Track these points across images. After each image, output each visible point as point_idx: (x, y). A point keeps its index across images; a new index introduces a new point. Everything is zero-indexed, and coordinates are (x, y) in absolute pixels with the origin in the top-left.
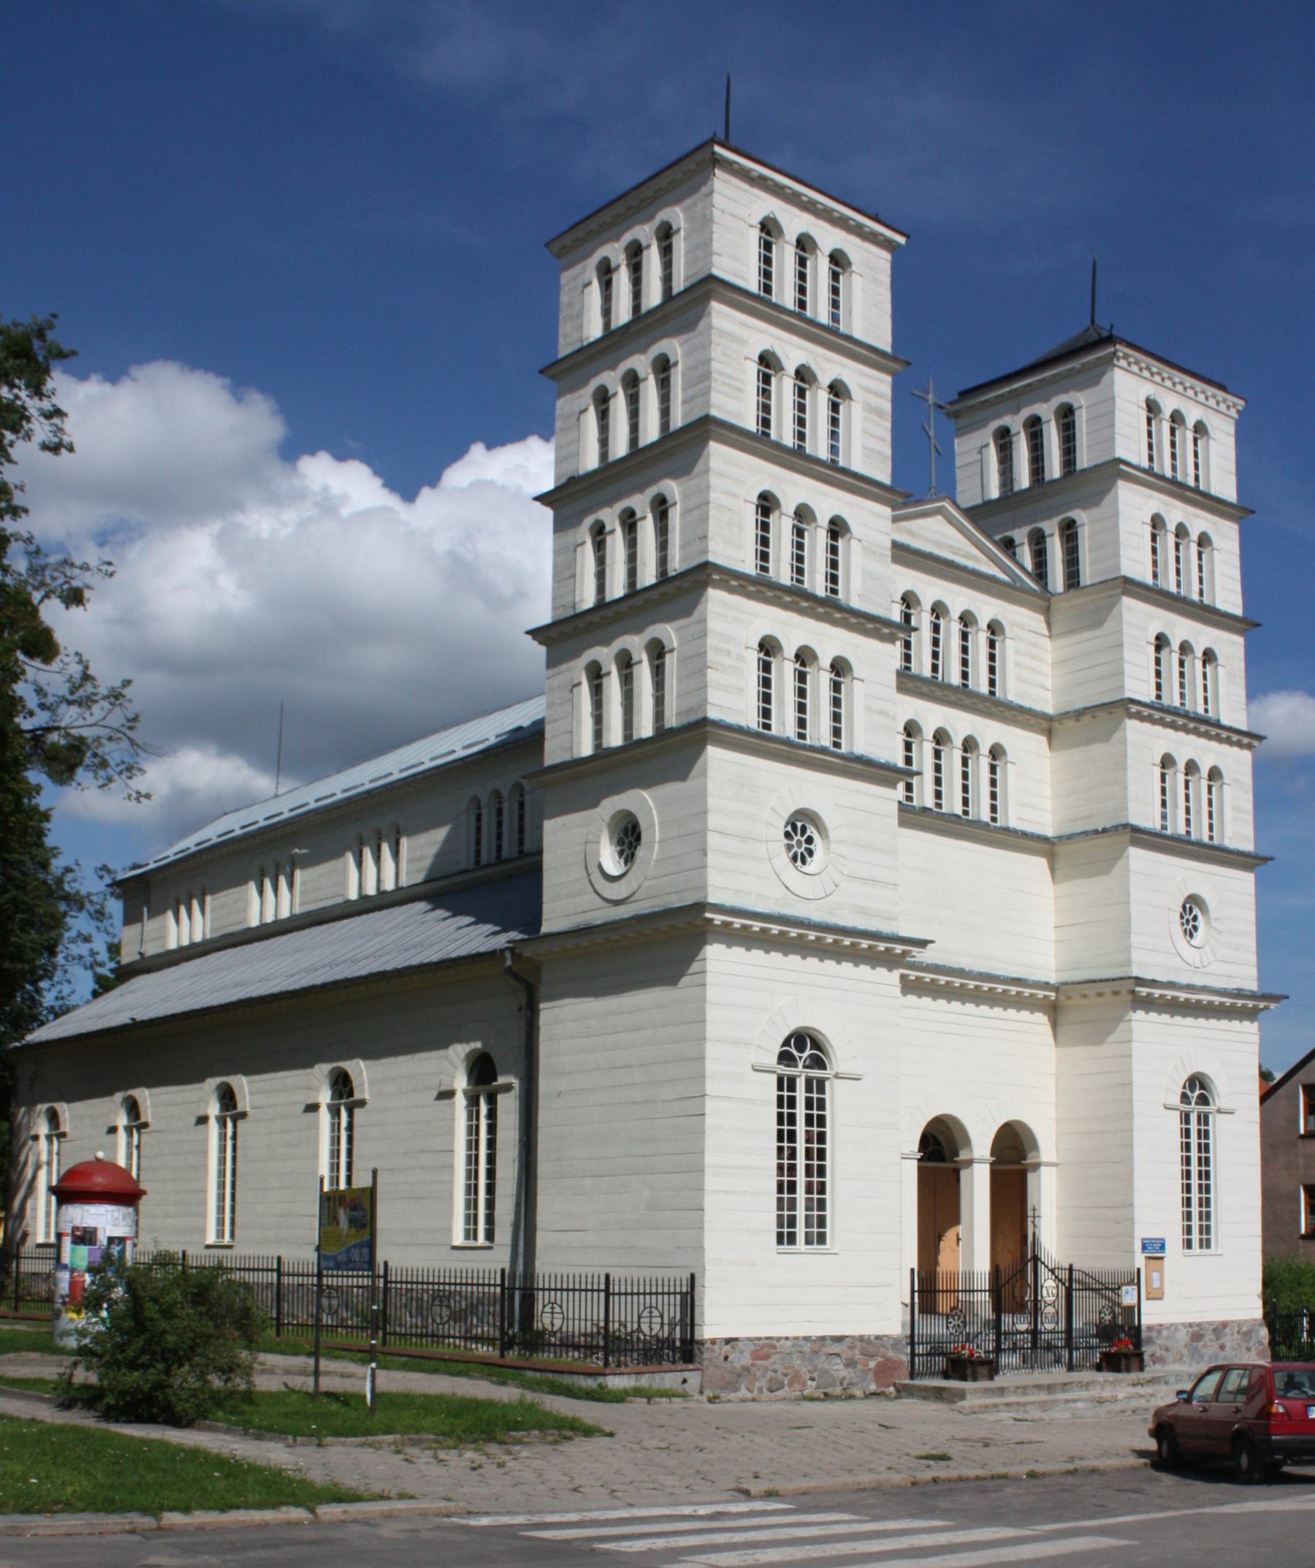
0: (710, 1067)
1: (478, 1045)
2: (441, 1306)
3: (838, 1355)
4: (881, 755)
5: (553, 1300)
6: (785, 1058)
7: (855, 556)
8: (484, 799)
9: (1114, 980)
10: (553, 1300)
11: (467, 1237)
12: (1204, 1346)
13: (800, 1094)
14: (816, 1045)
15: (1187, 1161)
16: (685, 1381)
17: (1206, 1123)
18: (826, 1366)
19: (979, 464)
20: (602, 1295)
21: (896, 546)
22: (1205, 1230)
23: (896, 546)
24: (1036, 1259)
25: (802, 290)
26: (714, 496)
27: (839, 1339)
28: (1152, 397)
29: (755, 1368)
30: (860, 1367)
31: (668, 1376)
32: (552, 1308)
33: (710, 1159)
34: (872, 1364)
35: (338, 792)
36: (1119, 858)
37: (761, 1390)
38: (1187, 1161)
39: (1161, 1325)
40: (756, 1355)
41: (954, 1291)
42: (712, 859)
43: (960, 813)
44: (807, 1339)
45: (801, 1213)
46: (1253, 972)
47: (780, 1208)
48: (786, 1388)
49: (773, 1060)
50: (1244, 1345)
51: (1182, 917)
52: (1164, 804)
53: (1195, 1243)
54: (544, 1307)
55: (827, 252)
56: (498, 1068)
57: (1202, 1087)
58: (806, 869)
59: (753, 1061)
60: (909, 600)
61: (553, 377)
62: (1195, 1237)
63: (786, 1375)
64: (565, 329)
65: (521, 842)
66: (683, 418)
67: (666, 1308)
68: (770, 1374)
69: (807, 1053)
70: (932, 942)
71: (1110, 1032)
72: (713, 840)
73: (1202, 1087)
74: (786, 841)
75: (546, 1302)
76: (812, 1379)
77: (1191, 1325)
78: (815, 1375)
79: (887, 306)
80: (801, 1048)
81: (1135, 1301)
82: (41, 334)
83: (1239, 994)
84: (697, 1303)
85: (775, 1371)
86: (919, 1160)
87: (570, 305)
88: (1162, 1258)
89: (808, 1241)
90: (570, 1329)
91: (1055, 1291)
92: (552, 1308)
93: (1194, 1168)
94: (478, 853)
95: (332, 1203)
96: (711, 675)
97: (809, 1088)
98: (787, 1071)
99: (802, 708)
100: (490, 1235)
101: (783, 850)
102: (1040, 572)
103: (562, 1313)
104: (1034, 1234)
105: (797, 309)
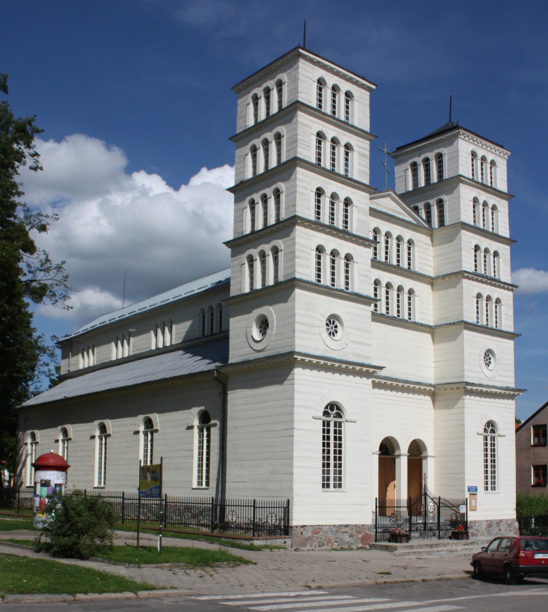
0: (296, 417)
1: (203, 408)
3: (346, 532)
5: (232, 510)
6: (326, 413)
7: (355, 214)
8: (206, 309)
9: (457, 383)
11: (198, 484)
12: (493, 529)
13: (332, 428)
14: (338, 408)
15: (486, 455)
16: (285, 542)
17: (494, 440)
18: (342, 537)
19: (404, 177)
20: (252, 508)
21: (371, 209)
22: (493, 483)
23: (371, 209)
24: (426, 494)
26: (298, 189)
27: (347, 526)
29: (313, 538)
30: (355, 537)
32: (232, 513)
33: (295, 454)
34: (360, 536)
35: (148, 306)
36: (459, 334)
37: (315, 546)
38: (486, 455)
39: (475, 521)
40: (314, 532)
41: (393, 507)
42: (297, 334)
44: (334, 526)
45: (332, 475)
46: (513, 380)
47: (323, 473)
48: (326, 545)
49: (321, 414)
50: (509, 529)
51: (485, 358)
52: (478, 313)
53: (489, 488)
55: (344, 92)
56: (211, 417)
57: (492, 426)
59: (313, 415)
60: (376, 231)
62: (489, 486)
63: (325, 540)
64: (239, 122)
65: (221, 327)
67: (278, 513)
68: (319, 540)
69: (335, 411)
70: (385, 367)
71: (456, 404)
72: (297, 327)
73: (492, 426)
75: (230, 510)
76: (336, 542)
77: (487, 521)
78: (337, 540)
80: (332, 410)
81: (465, 511)
82: (30, 123)
84: (290, 511)
85: (321, 539)
86: (379, 455)
87: (241, 112)
88: (476, 494)
89: (335, 487)
91: (433, 507)
92: (232, 513)
94: (203, 331)
96: (297, 260)
97: (335, 426)
101: (325, 330)
102: (429, 220)
103: (236, 515)
104: (425, 484)
105: (332, 115)
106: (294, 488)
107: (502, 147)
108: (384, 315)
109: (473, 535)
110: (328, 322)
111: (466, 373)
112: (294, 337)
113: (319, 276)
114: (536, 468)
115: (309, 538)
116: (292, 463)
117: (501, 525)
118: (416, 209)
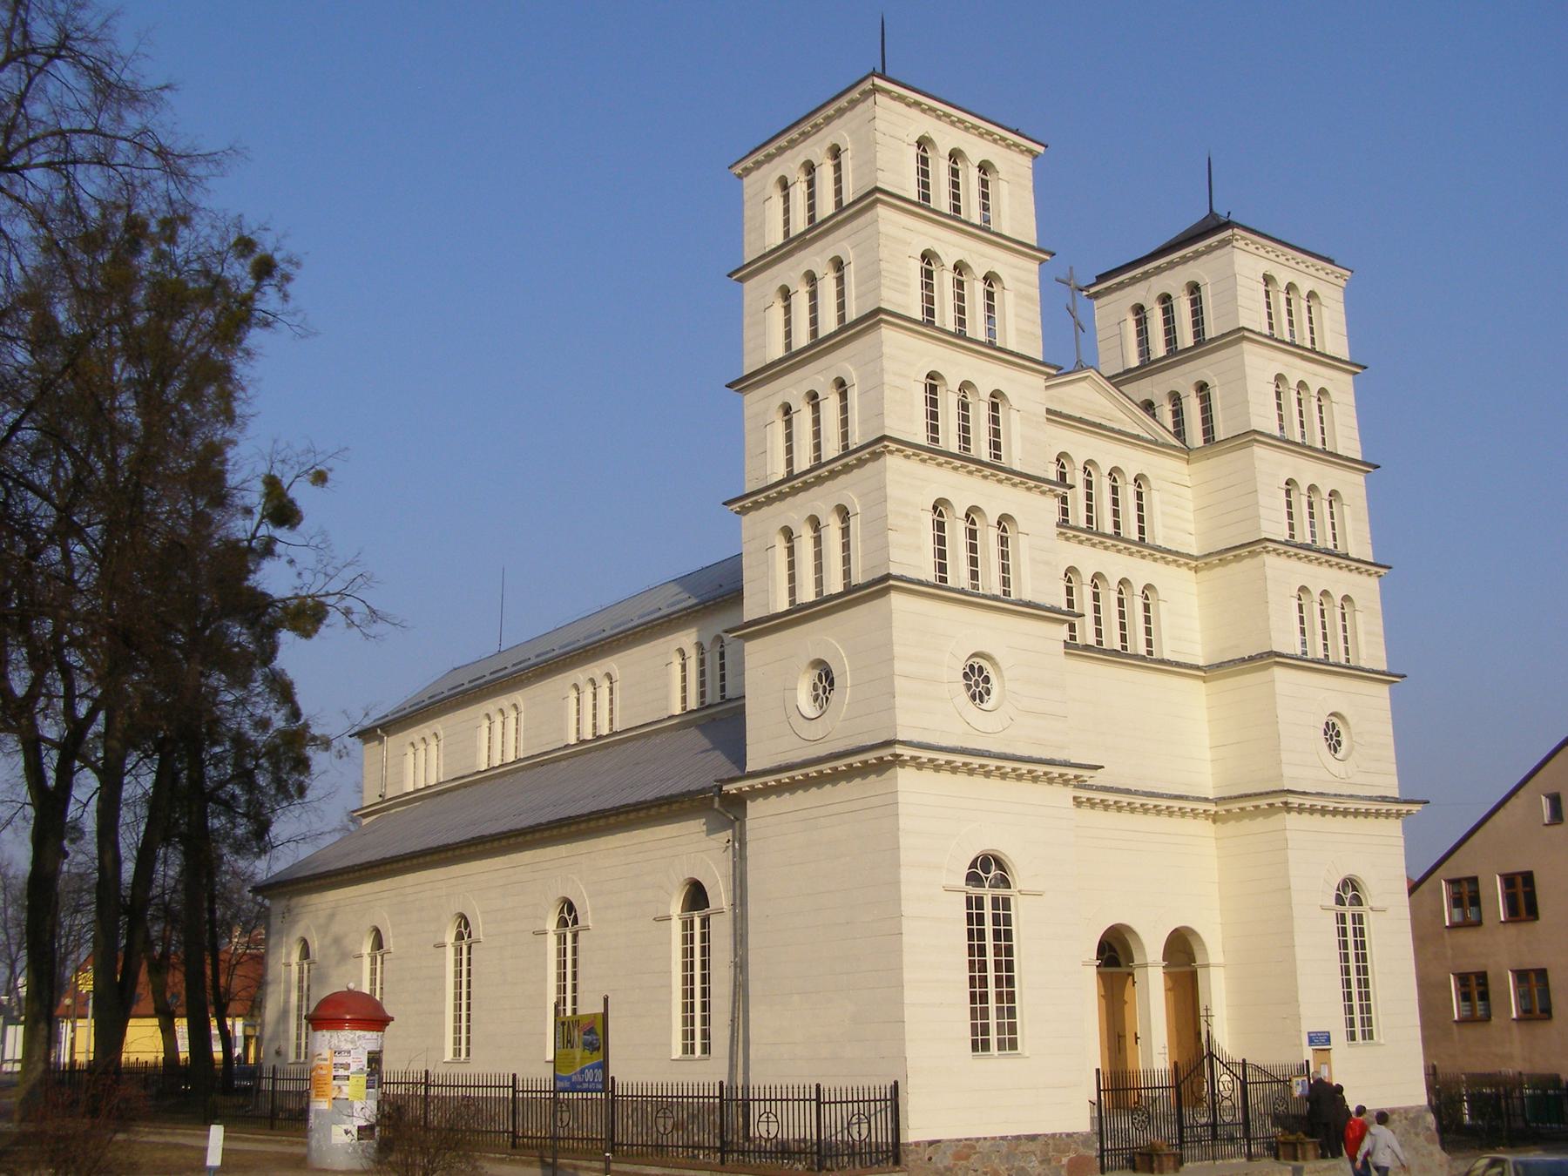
4: (1047, 601)
5: (768, 1110)
6: (973, 879)
13: (988, 912)
17: (1361, 922)
20: (814, 1103)
24: (1211, 1055)
30: (1053, 1163)
32: (768, 1117)
34: (1065, 1160)
42: (899, 701)
46: (1394, 780)
50: (1412, 1131)
51: (1326, 734)
52: (1303, 631)
54: (760, 1116)
57: (1355, 888)
58: (984, 706)
60: (1062, 458)
65: (723, 688)
73: (1355, 888)
75: (762, 1112)
83: (1384, 799)
88: (1329, 1050)
90: (785, 1136)
91: (1230, 1085)
95: (566, 1027)
98: (975, 891)
99: (974, 562)
100: (706, 1049)
101: (963, 689)
102: (1179, 432)
104: (1208, 1032)
110: (967, 670)
111: (1287, 771)
114: (1463, 979)
117: (1394, 1121)
118: (1148, 406)
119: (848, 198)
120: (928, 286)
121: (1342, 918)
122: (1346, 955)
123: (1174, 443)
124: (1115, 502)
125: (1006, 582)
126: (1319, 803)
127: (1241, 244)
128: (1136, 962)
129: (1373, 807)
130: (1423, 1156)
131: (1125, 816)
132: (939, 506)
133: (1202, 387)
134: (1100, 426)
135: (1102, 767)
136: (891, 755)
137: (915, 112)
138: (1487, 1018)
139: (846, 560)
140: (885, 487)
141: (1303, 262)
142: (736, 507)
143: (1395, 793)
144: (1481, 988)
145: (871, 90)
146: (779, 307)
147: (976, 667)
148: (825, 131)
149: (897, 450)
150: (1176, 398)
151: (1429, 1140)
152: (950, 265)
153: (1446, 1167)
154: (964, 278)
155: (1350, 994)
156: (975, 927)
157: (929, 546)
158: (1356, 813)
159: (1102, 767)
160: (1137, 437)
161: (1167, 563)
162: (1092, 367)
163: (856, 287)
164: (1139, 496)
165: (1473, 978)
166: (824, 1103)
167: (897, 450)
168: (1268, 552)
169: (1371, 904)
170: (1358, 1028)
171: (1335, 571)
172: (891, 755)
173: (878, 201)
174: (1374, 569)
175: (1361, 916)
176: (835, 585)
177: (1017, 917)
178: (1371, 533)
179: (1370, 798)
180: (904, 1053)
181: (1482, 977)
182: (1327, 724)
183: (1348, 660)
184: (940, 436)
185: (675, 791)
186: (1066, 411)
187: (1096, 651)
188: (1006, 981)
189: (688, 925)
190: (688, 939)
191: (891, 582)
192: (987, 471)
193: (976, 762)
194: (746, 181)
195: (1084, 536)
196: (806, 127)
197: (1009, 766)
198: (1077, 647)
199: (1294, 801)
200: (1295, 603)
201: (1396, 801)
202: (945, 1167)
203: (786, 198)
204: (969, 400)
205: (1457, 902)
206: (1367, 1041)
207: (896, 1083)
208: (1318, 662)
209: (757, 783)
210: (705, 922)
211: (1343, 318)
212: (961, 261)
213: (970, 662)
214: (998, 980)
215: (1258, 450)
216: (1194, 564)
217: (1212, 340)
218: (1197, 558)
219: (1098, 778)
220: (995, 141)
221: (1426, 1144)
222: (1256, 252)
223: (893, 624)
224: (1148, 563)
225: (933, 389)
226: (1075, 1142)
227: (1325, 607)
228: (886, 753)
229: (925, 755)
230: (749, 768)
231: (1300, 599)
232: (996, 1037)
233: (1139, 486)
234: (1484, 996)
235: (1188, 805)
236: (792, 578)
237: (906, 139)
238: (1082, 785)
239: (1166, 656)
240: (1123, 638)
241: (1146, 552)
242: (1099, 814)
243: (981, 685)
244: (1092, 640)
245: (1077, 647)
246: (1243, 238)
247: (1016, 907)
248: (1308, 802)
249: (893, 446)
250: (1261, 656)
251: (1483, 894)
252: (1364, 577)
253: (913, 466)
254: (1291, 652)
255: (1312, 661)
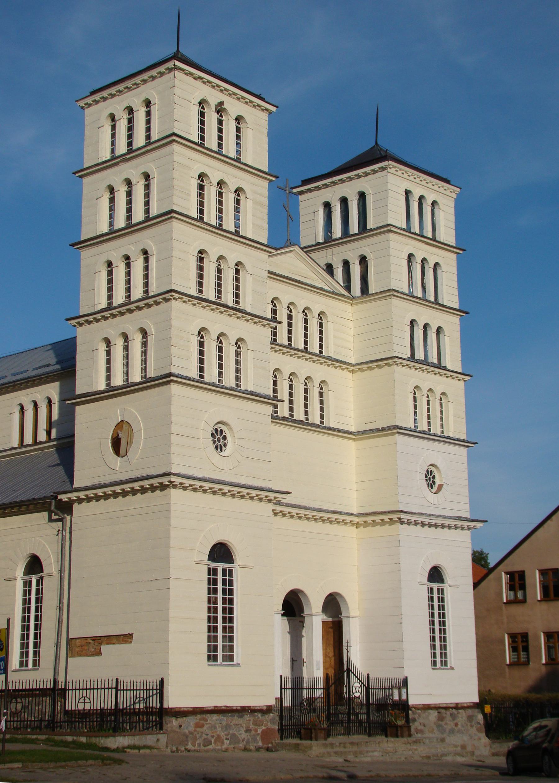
0: (172, 563)
2: (17, 703)
4: (262, 391)
5: (85, 695)
10: (85, 695)
12: (446, 724)
13: (220, 577)
15: (432, 615)
16: (158, 740)
17: (443, 594)
20: (114, 690)
22: (444, 655)
24: (349, 670)
25: (221, 138)
26: (175, 253)
28: (408, 189)
29: (196, 733)
30: (253, 732)
31: (149, 737)
32: (84, 700)
33: (172, 613)
34: (259, 731)
37: (199, 745)
38: (432, 615)
42: (173, 449)
43: (303, 419)
45: (220, 644)
46: (467, 507)
47: (209, 641)
48: (213, 744)
50: (469, 724)
51: (426, 477)
52: (415, 413)
54: (79, 700)
58: (222, 454)
60: (274, 301)
61: (404, 679)
63: (213, 737)
64: (88, 151)
66: (158, 209)
68: (204, 736)
72: (174, 439)
74: (212, 439)
75: (81, 696)
76: (227, 739)
78: (229, 737)
79: (266, 146)
83: (460, 518)
85: (207, 735)
91: (360, 689)
92: (84, 700)
93: (436, 619)
96: (174, 350)
97: (224, 574)
99: (220, 366)
100: (36, 663)
101: (212, 442)
102: (348, 288)
103: (90, 702)
104: (348, 656)
106: (170, 661)
107: (447, 181)
108: (288, 418)
109: (418, 731)
110: (214, 432)
112: (170, 453)
113: (202, 369)
114: (513, 637)
115: (191, 733)
116: (168, 627)
118: (329, 269)
119: (154, 137)
120: (201, 195)
121: (431, 590)
122: (433, 613)
123: (344, 294)
124: (306, 328)
125: (238, 379)
126: (420, 519)
127: (393, 170)
128: (305, 613)
129: (453, 523)
130: (475, 739)
131: (303, 522)
132: (201, 332)
133: (363, 260)
134: (299, 282)
135: (290, 493)
136: (168, 481)
137: (199, 83)
138: (527, 663)
139: (145, 361)
140: (170, 320)
141: (430, 182)
142: (74, 322)
143: (467, 515)
144: (524, 644)
145: (172, 68)
146: (107, 195)
147: (219, 430)
148: (142, 88)
149: (179, 298)
150: (346, 264)
151: (479, 730)
152: (215, 183)
153: (488, 748)
154: (223, 190)
155: (434, 637)
156: (212, 586)
157: (195, 356)
158: (443, 526)
159: (290, 493)
160: (321, 289)
161: (336, 367)
162: (296, 245)
163: (158, 194)
164: (320, 325)
165: (520, 637)
166: (120, 690)
167: (179, 298)
168: (397, 364)
169: (449, 582)
170: (438, 659)
171: (437, 377)
172: (168, 481)
173: (174, 141)
174: (461, 376)
175: (442, 590)
176: (136, 377)
177: (237, 582)
178: (462, 353)
179: (451, 518)
180: (168, 661)
181: (525, 636)
182: (427, 471)
183: (442, 432)
184: (204, 289)
185: (24, 497)
186: (278, 272)
187: (289, 420)
188: (229, 620)
189: (27, 584)
190: (27, 593)
191: (172, 378)
192: (231, 312)
193: (217, 487)
194: (87, 111)
195: (285, 350)
196: (129, 83)
197: (236, 490)
198: (278, 418)
199: (405, 517)
200: (411, 396)
201: (468, 520)
202: (189, 732)
203: (114, 127)
204: (222, 267)
205: (511, 587)
206: (444, 667)
207: (162, 679)
208: (424, 433)
209: (82, 495)
210: (40, 582)
211: (453, 218)
212: (222, 180)
213: (215, 427)
214: (224, 619)
215: (395, 301)
216: (351, 368)
217: (371, 230)
218: (353, 365)
219: (288, 499)
220: (247, 103)
221: (477, 733)
222: (402, 175)
223: (172, 403)
224: (324, 367)
225: (201, 260)
226: (266, 720)
227: (430, 398)
228: (165, 480)
229: (188, 482)
230: (75, 485)
231: (415, 393)
232: (222, 653)
233: (321, 319)
234: (526, 649)
235: (341, 517)
236: (108, 370)
237: (193, 101)
238: (279, 503)
239: (332, 425)
240: (306, 413)
241: (323, 360)
242: (287, 520)
243: (221, 440)
244: (287, 414)
245: (278, 418)
246: (394, 167)
247: (237, 575)
248: (413, 518)
249: (176, 296)
250: (390, 428)
251: (528, 581)
252: (455, 381)
253: (188, 307)
254: (407, 426)
255: (420, 432)
